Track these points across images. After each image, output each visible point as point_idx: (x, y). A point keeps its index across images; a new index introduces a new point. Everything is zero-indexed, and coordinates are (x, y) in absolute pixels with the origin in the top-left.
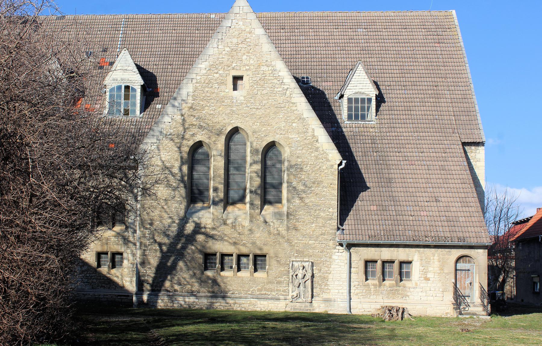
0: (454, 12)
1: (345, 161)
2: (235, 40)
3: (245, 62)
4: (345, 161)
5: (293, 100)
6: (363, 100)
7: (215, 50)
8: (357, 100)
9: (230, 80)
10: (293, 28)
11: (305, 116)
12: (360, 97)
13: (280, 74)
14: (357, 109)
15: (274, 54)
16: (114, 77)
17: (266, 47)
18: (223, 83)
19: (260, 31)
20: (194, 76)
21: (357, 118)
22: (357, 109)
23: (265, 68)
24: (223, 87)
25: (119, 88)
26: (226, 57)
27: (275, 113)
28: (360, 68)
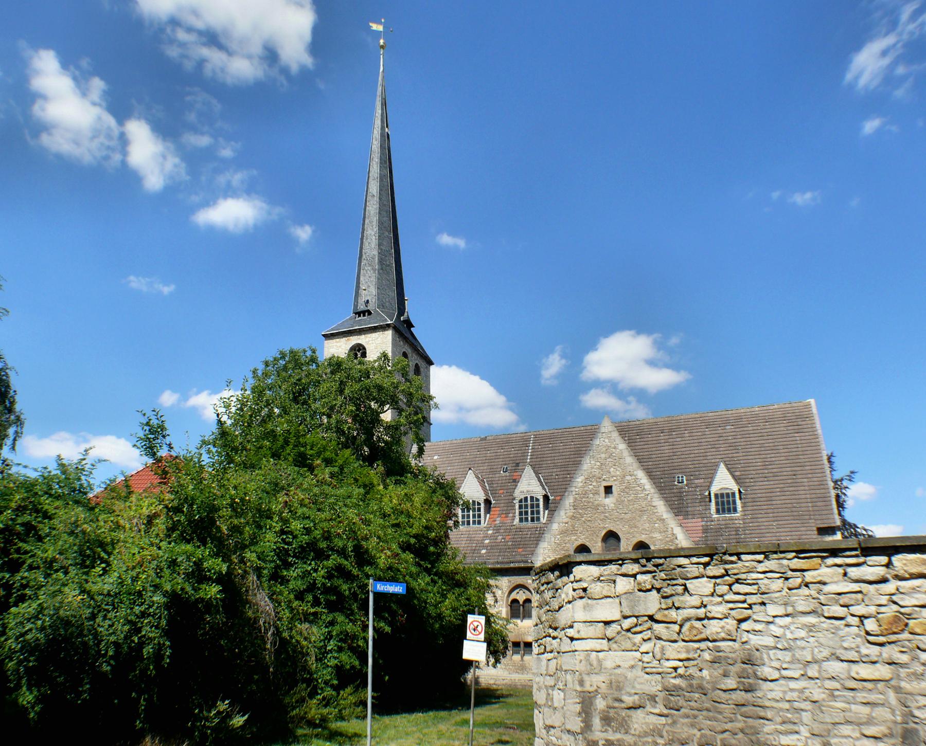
0: (812, 401)
1: (287, 700)
2: (603, 456)
3: (613, 474)
4: (287, 700)
5: (654, 504)
6: (728, 494)
7: (588, 465)
8: (722, 495)
9: (602, 490)
10: (671, 430)
11: (664, 517)
12: (725, 492)
13: (642, 481)
14: (723, 503)
15: (636, 465)
16: (521, 489)
17: (629, 459)
18: (597, 493)
19: (622, 446)
20: (573, 489)
21: (724, 511)
22: (723, 503)
23: (628, 478)
24: (597, 496)
25: (526, 499)
26: (598, 471)
27: (640, 516)
28: (722, 465)
